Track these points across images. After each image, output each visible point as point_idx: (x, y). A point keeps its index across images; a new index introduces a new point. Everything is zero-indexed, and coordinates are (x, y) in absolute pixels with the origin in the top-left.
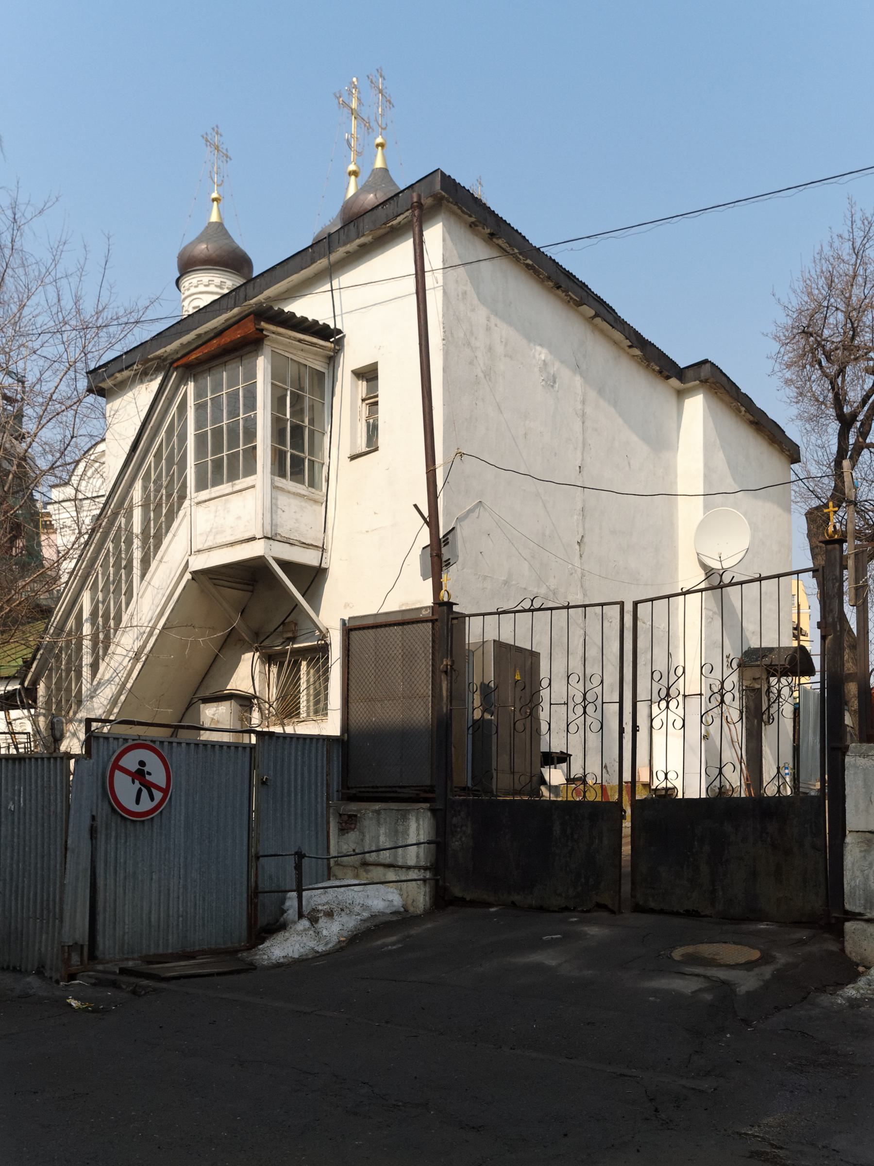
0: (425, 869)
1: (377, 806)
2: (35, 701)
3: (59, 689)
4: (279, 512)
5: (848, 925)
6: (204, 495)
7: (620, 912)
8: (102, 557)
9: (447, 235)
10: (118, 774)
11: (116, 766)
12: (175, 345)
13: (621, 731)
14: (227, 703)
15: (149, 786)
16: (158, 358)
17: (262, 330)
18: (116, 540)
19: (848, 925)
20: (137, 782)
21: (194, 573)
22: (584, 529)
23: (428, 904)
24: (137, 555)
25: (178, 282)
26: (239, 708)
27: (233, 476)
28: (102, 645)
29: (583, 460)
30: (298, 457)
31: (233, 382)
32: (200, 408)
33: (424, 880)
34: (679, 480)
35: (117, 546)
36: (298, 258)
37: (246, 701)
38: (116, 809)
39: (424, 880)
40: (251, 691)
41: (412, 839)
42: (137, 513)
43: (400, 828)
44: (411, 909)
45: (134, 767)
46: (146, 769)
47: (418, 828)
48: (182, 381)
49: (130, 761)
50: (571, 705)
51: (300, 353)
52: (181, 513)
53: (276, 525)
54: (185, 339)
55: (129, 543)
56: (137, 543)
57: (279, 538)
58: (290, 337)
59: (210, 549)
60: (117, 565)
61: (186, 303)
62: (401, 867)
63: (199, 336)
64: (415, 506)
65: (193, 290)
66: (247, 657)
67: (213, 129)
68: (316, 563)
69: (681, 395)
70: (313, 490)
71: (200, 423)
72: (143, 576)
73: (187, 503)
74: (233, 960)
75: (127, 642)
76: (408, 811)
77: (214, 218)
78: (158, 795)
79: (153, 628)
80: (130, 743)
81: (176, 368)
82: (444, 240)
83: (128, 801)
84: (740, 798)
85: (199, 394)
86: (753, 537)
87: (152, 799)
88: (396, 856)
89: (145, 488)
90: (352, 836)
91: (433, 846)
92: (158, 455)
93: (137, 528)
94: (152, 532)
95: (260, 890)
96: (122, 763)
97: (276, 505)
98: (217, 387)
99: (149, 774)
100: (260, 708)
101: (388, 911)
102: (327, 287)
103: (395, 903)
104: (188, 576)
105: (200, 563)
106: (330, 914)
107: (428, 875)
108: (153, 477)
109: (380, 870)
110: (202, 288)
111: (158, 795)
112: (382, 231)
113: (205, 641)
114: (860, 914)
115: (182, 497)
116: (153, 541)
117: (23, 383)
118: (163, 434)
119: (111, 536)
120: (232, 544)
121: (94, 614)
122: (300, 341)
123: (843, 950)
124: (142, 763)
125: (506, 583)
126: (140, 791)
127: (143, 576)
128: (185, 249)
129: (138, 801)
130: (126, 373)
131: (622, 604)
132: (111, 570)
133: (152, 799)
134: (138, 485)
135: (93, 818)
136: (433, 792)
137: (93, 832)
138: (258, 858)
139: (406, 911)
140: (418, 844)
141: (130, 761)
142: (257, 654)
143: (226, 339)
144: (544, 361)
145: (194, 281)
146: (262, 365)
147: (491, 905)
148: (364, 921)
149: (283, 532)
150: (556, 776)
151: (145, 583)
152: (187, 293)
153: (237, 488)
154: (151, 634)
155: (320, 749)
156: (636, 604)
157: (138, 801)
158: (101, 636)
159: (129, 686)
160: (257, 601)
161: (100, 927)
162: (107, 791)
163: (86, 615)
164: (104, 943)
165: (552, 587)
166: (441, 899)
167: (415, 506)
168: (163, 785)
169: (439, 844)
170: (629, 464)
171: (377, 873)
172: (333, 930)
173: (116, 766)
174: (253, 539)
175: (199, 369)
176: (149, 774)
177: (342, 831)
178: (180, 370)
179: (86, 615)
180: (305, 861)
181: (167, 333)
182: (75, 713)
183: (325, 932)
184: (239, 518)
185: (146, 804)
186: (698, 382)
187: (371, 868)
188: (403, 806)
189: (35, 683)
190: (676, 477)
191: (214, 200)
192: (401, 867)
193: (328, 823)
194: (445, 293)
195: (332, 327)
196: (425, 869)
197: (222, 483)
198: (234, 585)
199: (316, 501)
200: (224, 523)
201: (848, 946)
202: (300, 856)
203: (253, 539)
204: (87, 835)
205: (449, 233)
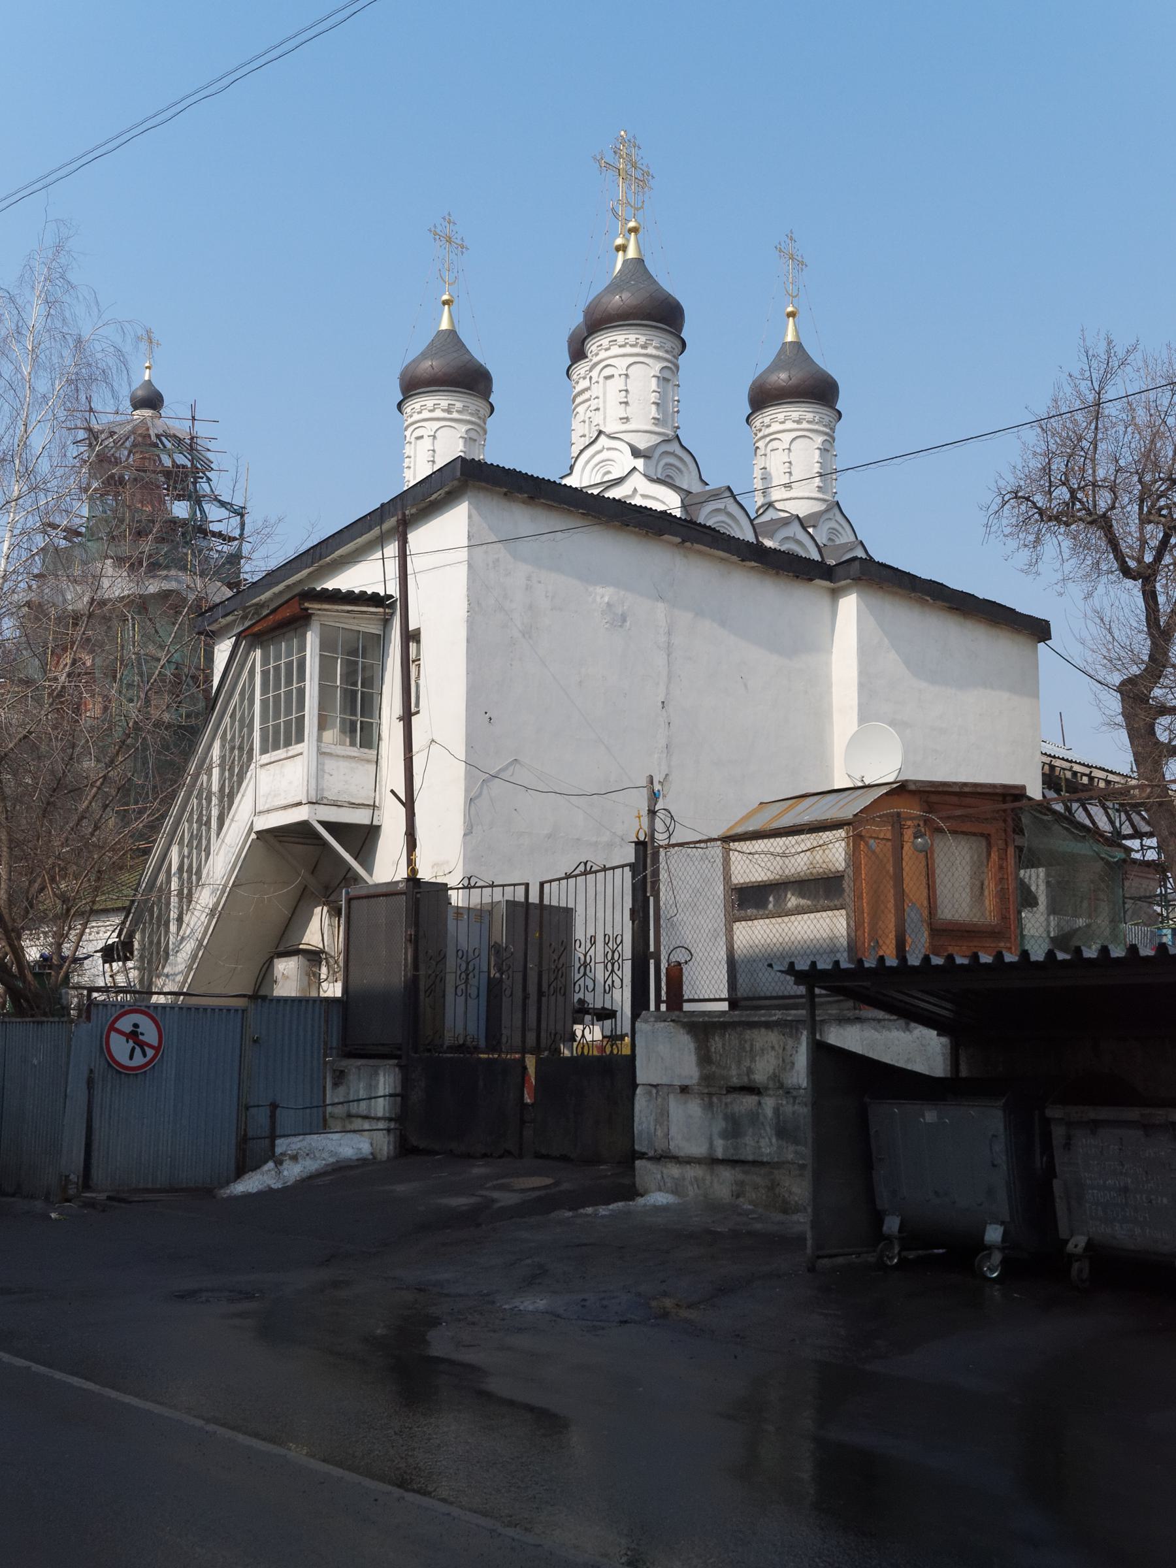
0: (390, 1119)
1: (360, 1062)
2: (132, 953)
3: (151, 943)
4: (326, 776)
5: (638, 1163)
6: (266, 758)
7: (521, 1156)
8: (186, 815)
9: (474, 512)
10: (113, 1034)
11: (111, 1028)
12: (268, 594)
13: (526, 997)
14: (295, 958)
15: (142, 1045)
16: (256, 604)
17: (307, 609)
18: (199, 797)
19: (638, 1163)
20: (131, 1042)
21: (257, 833)
22: (669, 766)
23: (392, 1153)
24: (215, 812)
25: (400, 406)
26: (307, 963)
27: (288, 744)
28: (187, 897)
29: (667, 694)
30: (356, 716)
31: (289, 653)
32: (265, 674)
33: (389, 1130)
34: (834, 689)
35: (200, 804)
36: (359, 524)
37: (314, 957)
38: (112, 1063)
39: (389, 1130)
40: (321, 946)
41: (381, 1093)
42: (216, 772)
43: (373, 1083)
44: (379, 1157)
45: (128, 1029)
46: (139, 1030)
47: (386, 1082)
48: (251, 648)
49: (125, 1024)
50: (476, 971)
51: (351, 621)
52: (249, 774)
53: (323, 789)
54: (276, 589)
55: (209, 801)
56: (215, 801)
57: (325, 801)
58: (337, 611)
59: (268, 811)
60: (199, 820)
61: (408, 433)
62: (373, 1118)
63: (288, 587)
64: (392, 791)
65: (416, 417)
66: (318, 910)
67: (444, 218)
68: (367, 822)
69: (835, 594)
70: (366, 750)
71: (265, 691)
72: (218, 835)
73: (253, 766)
74: (206, 1192)
75: (205, 898)
76: (378, 1067)
77: (445, 325)
78: (150, 1053)
79: (225, 886)
80: (127, 1008)
81: (245, 637)
82: (470, 517)
83: (123, 1059)
84: (593, 1056)
85: (265, 661)
86: (906, 753)
87: (145, 1055)
88: (369, 1107)
89: (223, 746)
90: (341, 1090)
91: (399, 1099)
92: (233, 716)
93: (215, 788)
94: (227, 791)
95: (250, 1134)
96: (117, 1025)
97: (323, 771)
98: (278, 657)
99: (142, 1034)
100: (327, 963)
101: (355, 1158)
102: (379, 555)
103: (364, 1151)
104: (253, 836)
105: (266, 823)
106: (294, 1158)
107: (392, 1125)
108: (229, 737)
109: (359, 1120)
110: (426, 414)
111: (150, 1053)
112: (423, 505)
113: (276, 898)
114: (645, 1154)
115: (250, 758)
116: (228, 797)
117: (242, 515)
118: (236, 696)
119: (195, 793)
120: (285, 807)
121: (180, 869)
122: (348, 612)
123: (634, 1184)
124: (136, 1026)
125: (549, 836)
126: (133, 1050)
127: (218, 835)
128: (407, 367)
129: (131, 1057)
130: (230, 618)
131: (527, 885)
132: (195, 825)
133: (145, 1055)
134: (217, 744)
135: (91, 1071)
136: (399, 1049)
137: (90, 1083)
138: (247, 1108)
139: (374, 1158)
140: (384, 1096)
141: (125, 1024)
142: (325, 909)
143: (279, 616)
144: (608, 603)
145: (417, 406)
146: (312, 639)
147: (438, 1153)
148: (327, 1165)
149: (330, 795)
150: (591, 1034)
151: (220, 841)
152: (410, 420)
153: (290, 754)
154: (223, 892)
155: (317, 1010)
156: (542, 885)
157: (131, 1057)
158: (185, 891)
159: (205, 943)
160: (313, 859)
161: (94, 1161)
162: (105, 1049)
163: (174, 869)
164: (97, 1175)
165: (620, 833)
166: (405, 1149)
167: (392, 791)
168: (156, 1044)
169: (401, 1097)
170: (746, 686)
171: (358, 1124)
172: (293, 1172)
173: (111, 1028)
174: (300, 804)
175: (265, 638)
176: (142, 1034)
177: (336, 1085)
178: (249, 638)
179: (174, 869)
180: (278, 1111)
181: (264, 581)
182: (163, 967)
183: (286, 1173)
184: (291, 783)
185: (139, 1060)
186: (849, 581)
187: (354, 1119)
188: (372, 1062)
189: (131, 935)
190: (830, 686)
191: (445, 303)
192: (373, 1118)
193: (325, 1078)
194: (470, 566)
195: (382, 594)
196: (390, 1119)
197: (278, 748)
198: (297, 840)
199: (368, 761)
200: (278, 788)
201: (637, 1179)
202: (274, 1106)
203: (300, 804)
204: (84, 1087)
205: (477, 509)
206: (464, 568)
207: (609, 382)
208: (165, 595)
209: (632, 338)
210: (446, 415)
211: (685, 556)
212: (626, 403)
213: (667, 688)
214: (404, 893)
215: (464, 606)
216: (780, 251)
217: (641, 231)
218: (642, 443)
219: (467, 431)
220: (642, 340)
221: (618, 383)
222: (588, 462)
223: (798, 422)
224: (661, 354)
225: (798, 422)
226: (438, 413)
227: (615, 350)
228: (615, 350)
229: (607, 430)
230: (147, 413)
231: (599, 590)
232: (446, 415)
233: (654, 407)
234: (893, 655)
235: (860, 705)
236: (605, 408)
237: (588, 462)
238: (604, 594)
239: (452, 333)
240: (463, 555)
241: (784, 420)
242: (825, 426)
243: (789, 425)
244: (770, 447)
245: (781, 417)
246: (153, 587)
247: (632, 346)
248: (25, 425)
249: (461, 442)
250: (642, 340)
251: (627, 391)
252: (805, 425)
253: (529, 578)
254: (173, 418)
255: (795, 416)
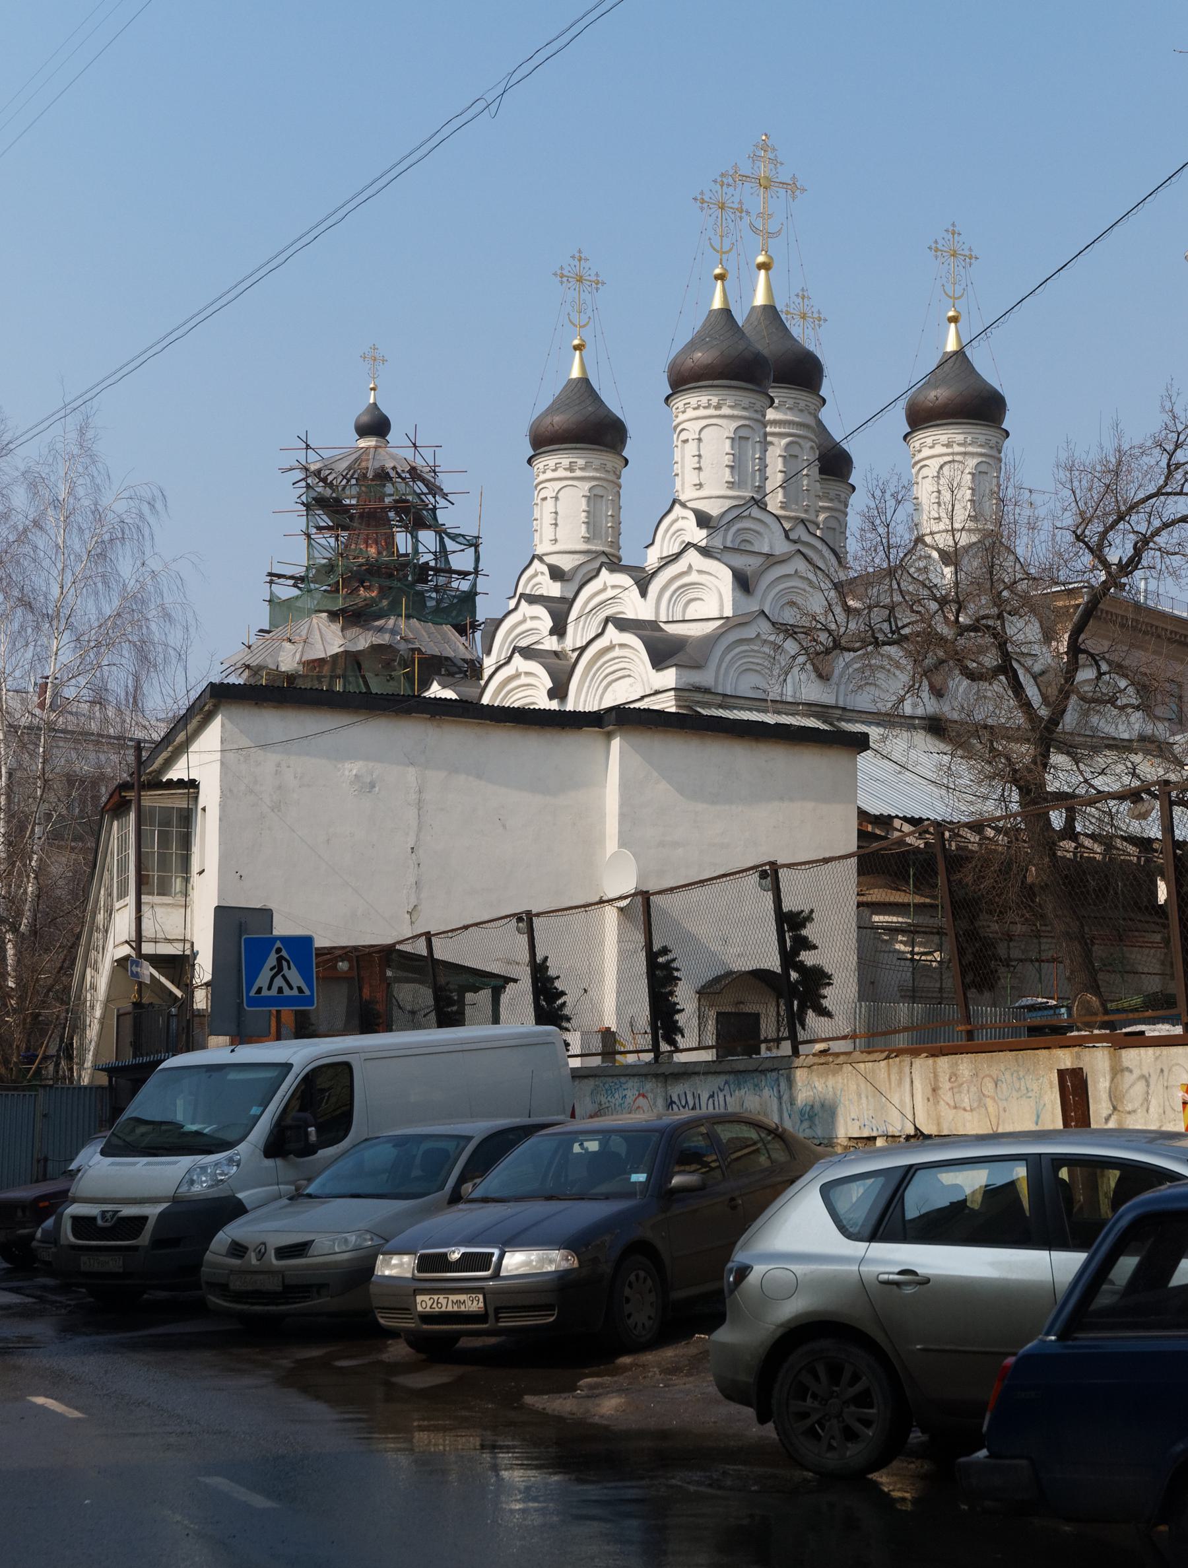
9: (226, 721)
22: (418, 899)
25: (530, 461)
28: (92, 1007)
67: (573, 257)
69: (609, 736)
77: (575, 373)
110: (550, 475)
117: (476, 546)
170: (504, 826)
194: (222, 763)
205: (229, 719)
206: (217, 766)
207: (686, 445)
208: (376, 649)
209: (704, 400)
210: (568, 474)
211: (439, 726)
212: (699, 469)
213: (417, 836)
214: (129, 1013)
215: (219, 791)
216: (937, 250)
217: (729, 277)
218: (714, 509)
219: (590, 489)
220: (715, 400)
221: (691, 448)
222: (667, 531)
223: (948, 445)
224: (736, 413)
225: (948, 445)
226: (561, 473)
227: (691, 413)
228: (691, 413)
229: (683, 498)
230: (369, 442)
231: (348, 765)
232: (568, 474)
233: (728, 470)
234: (663, 785)
235: (620, 832)
236: (683, 473)
237: (667, 531)
238: (352, 768)
239: (585, 382)
240: (218, 756)
241: (936, 444)
242: (981, 446)
243: (939, 450)
244: (920, 476)
245: (929, 441)
246: (363, 641)
247: (705, 408)
248: (62, 587)
249: (584, 501)
250: (715, 400)
251: (699, 456)
252: (957, 449)
253: (278, 765)
254: (396, 451)
255: (944, 439)
